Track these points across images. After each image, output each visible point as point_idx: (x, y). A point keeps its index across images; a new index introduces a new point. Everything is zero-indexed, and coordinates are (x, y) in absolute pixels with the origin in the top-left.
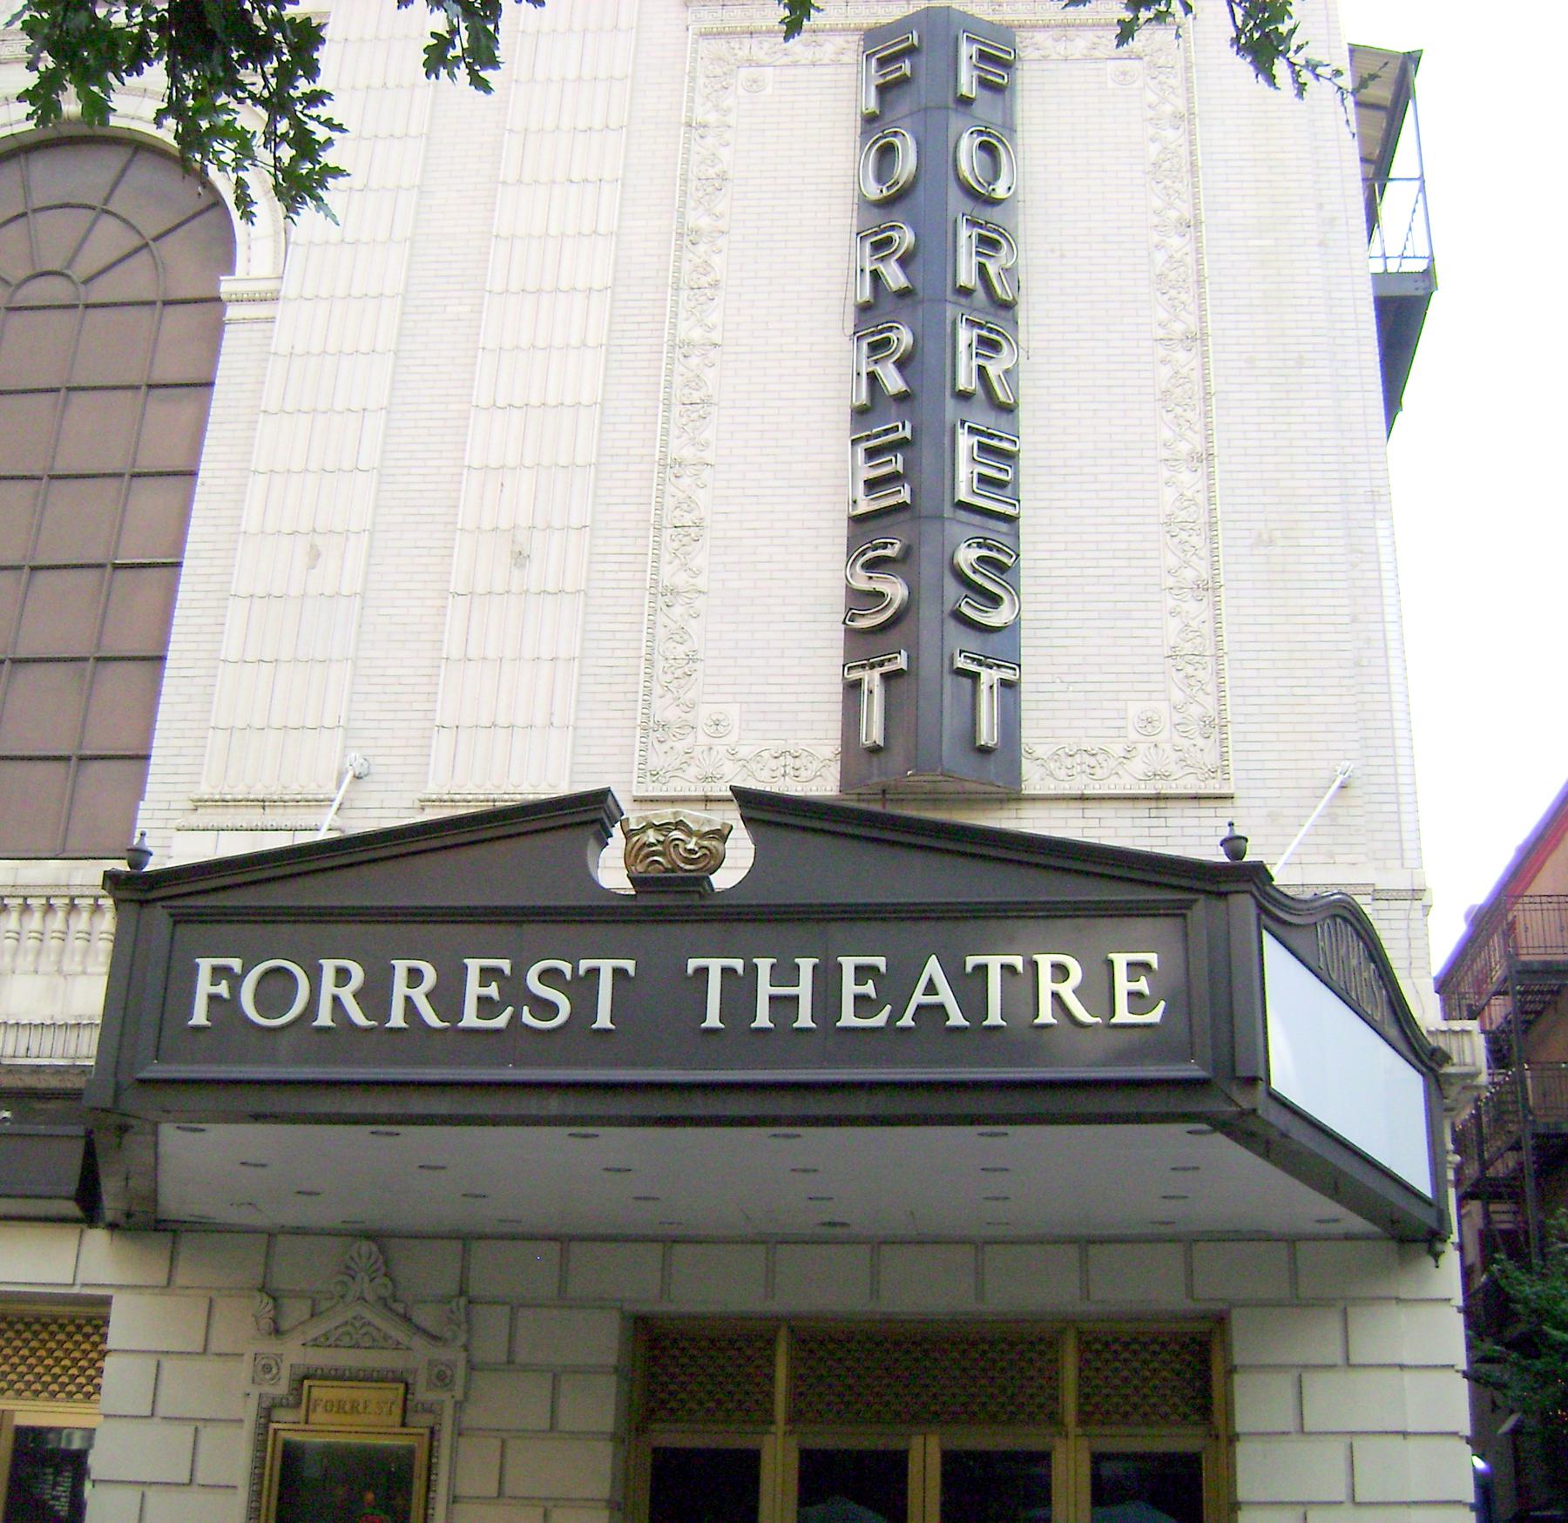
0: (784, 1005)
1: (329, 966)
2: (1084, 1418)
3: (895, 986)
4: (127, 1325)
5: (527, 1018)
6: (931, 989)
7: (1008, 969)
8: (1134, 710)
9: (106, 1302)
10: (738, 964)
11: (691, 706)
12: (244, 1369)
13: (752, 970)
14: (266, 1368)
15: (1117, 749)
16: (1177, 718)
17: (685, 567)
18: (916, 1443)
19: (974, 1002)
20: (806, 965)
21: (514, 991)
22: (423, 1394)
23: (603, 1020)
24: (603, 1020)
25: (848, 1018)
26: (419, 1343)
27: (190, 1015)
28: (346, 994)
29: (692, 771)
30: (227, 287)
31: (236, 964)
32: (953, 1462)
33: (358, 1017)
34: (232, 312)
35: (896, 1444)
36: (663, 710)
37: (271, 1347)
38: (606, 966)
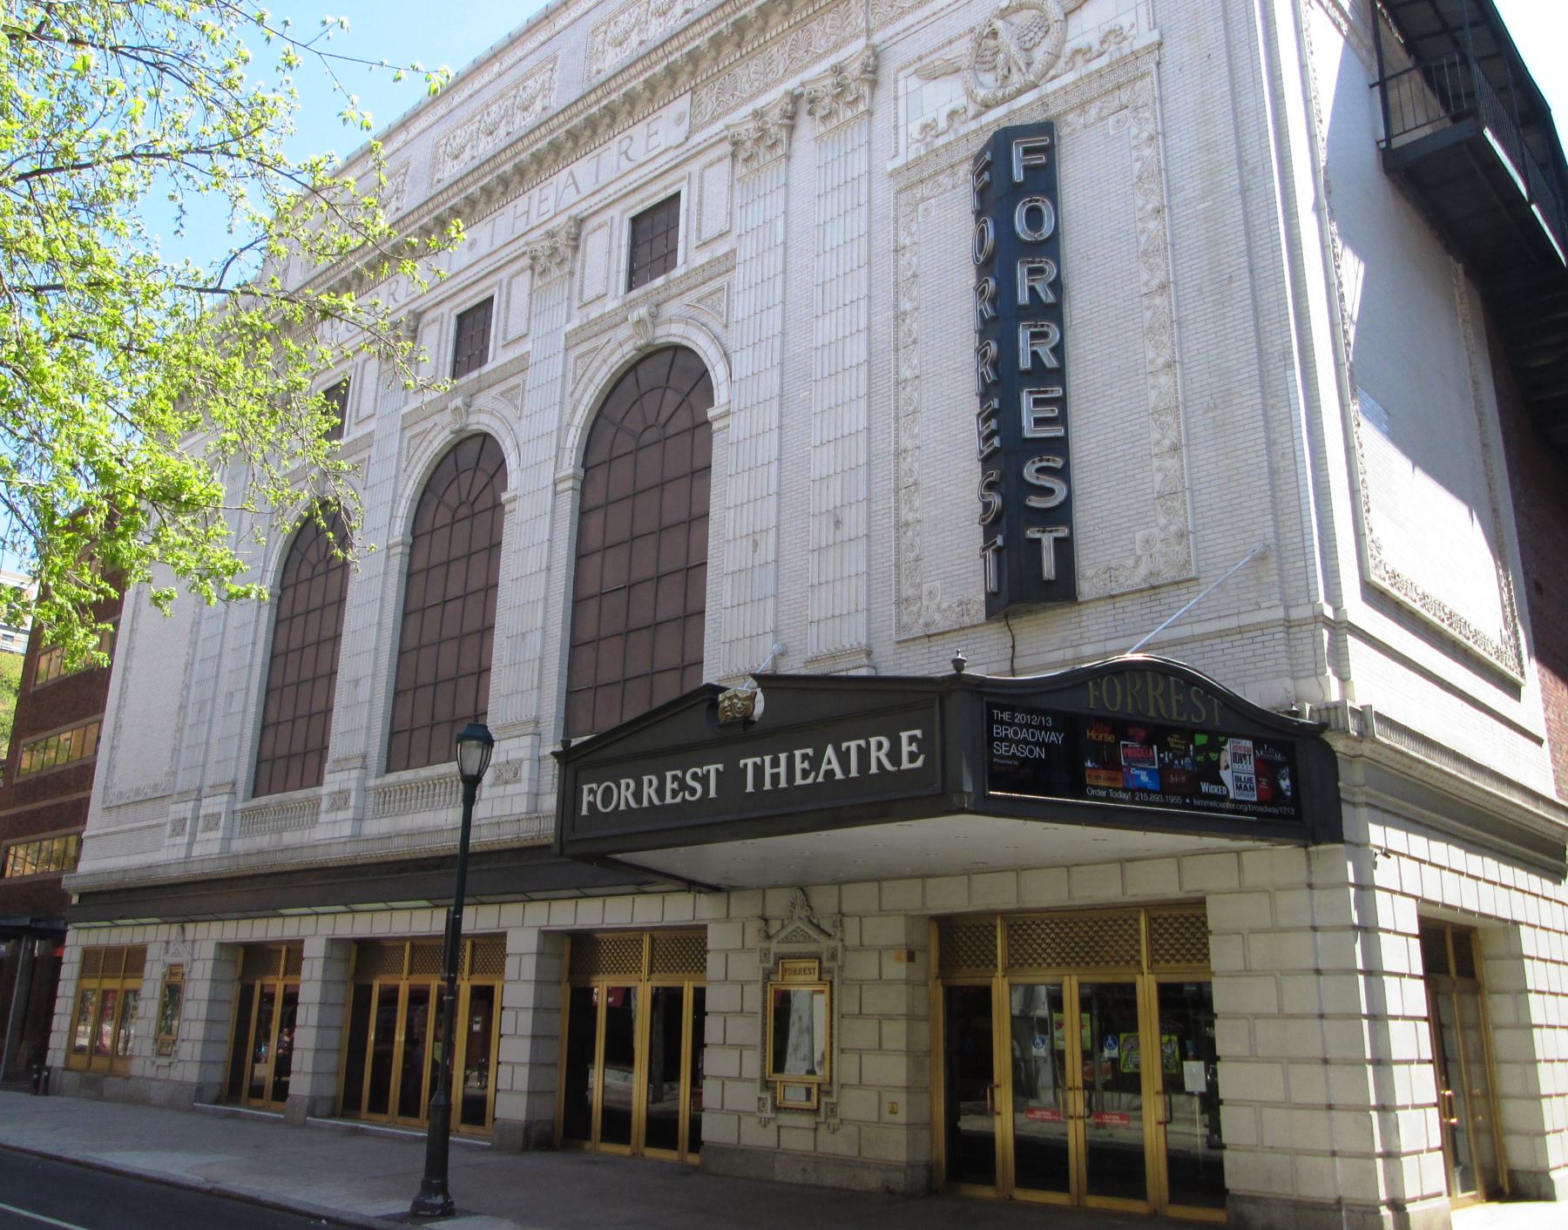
0: (775, 778)
1: (623, 782)
2: (1153, 961)
3: (815, 762)
4: (716, 938)
5: (688, 797)
6: (829, 762)
7: (859, 747)
8: (1139, 536)
9: (705, 927)
10: (862, 742)
11: (920, 585)
12: (757, 956)
13: (868, 744)
14: (765, 954)
15: (1131, 562)
16: (1163, 536)
17: (911, 509)
18: (1066, 979)
19: (845, 767)
20: (783, 757)
21: (683, 786)
22: (826, 964)
23: (712, 794)
24: (712, 794)
25: (799, 781)
26: (822, 938)
27: (869, 768)
28: (882, 755)
29: (921, 621)
30: (711, 413)
31: (594, 786)
32: (1163, 989)
33: (888, 766)
34: (715, 426)
35: (1125, 979)
36: (908, 591)
37: (766, 945)
38: (712, 768)
